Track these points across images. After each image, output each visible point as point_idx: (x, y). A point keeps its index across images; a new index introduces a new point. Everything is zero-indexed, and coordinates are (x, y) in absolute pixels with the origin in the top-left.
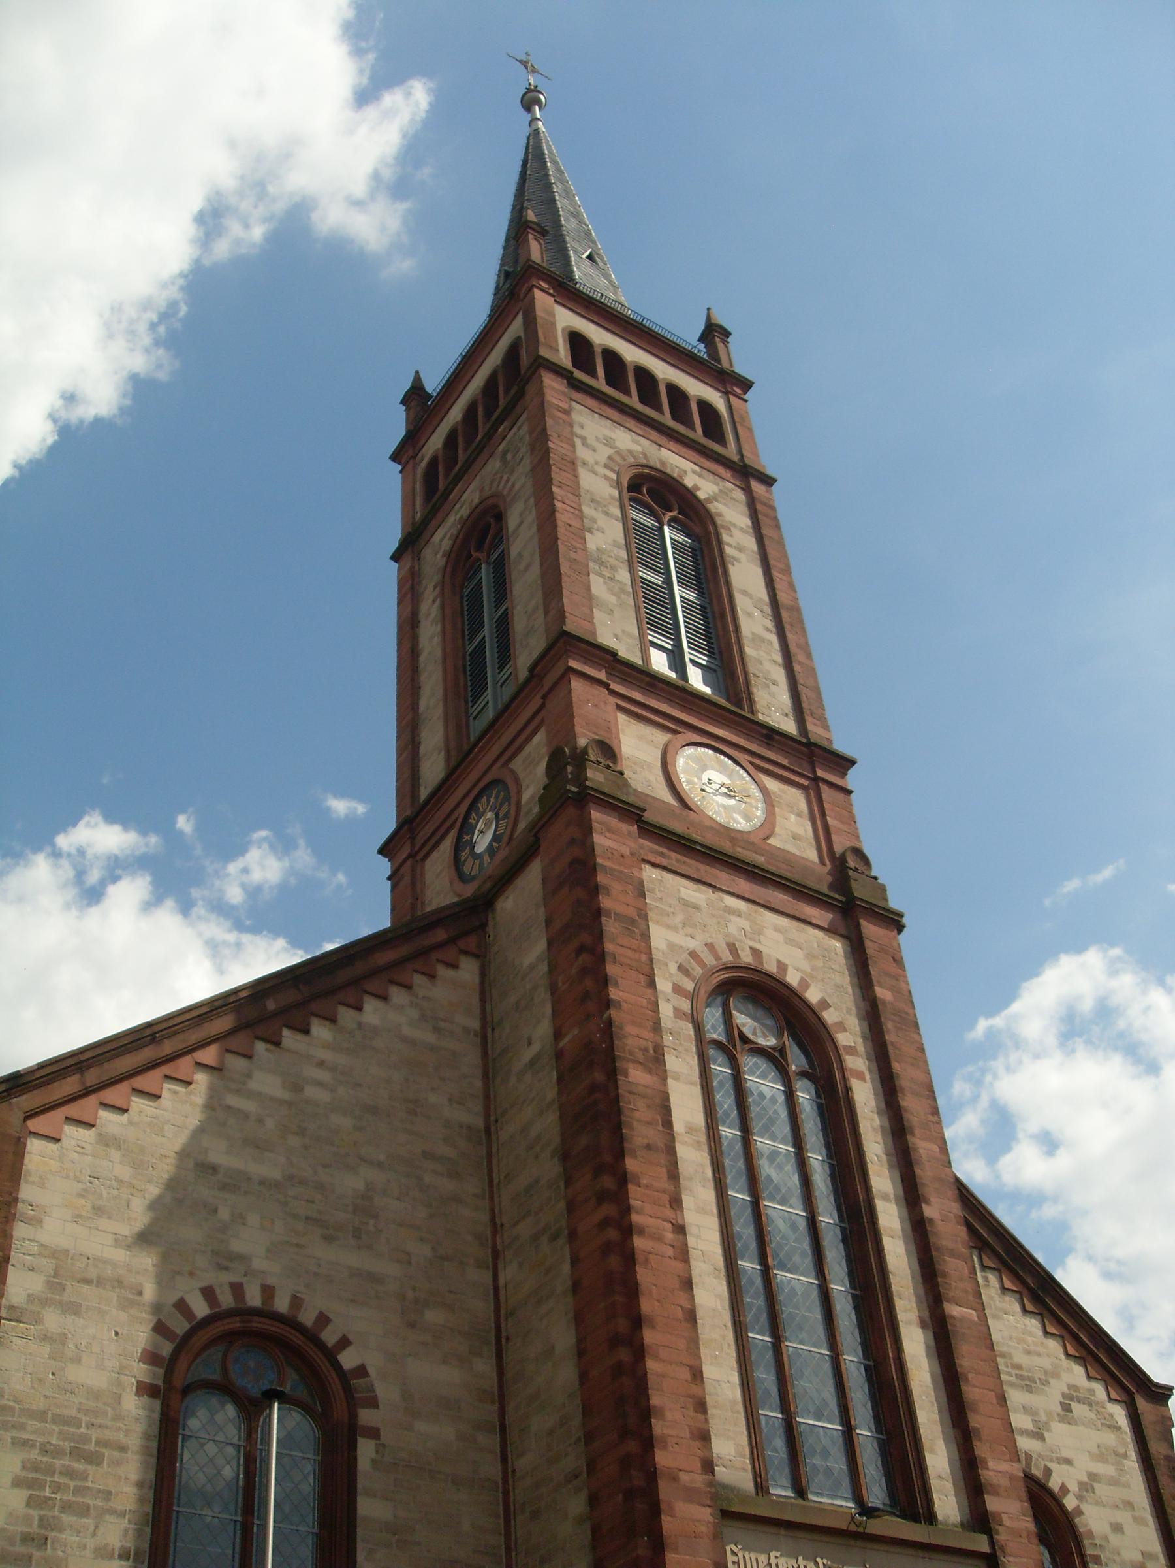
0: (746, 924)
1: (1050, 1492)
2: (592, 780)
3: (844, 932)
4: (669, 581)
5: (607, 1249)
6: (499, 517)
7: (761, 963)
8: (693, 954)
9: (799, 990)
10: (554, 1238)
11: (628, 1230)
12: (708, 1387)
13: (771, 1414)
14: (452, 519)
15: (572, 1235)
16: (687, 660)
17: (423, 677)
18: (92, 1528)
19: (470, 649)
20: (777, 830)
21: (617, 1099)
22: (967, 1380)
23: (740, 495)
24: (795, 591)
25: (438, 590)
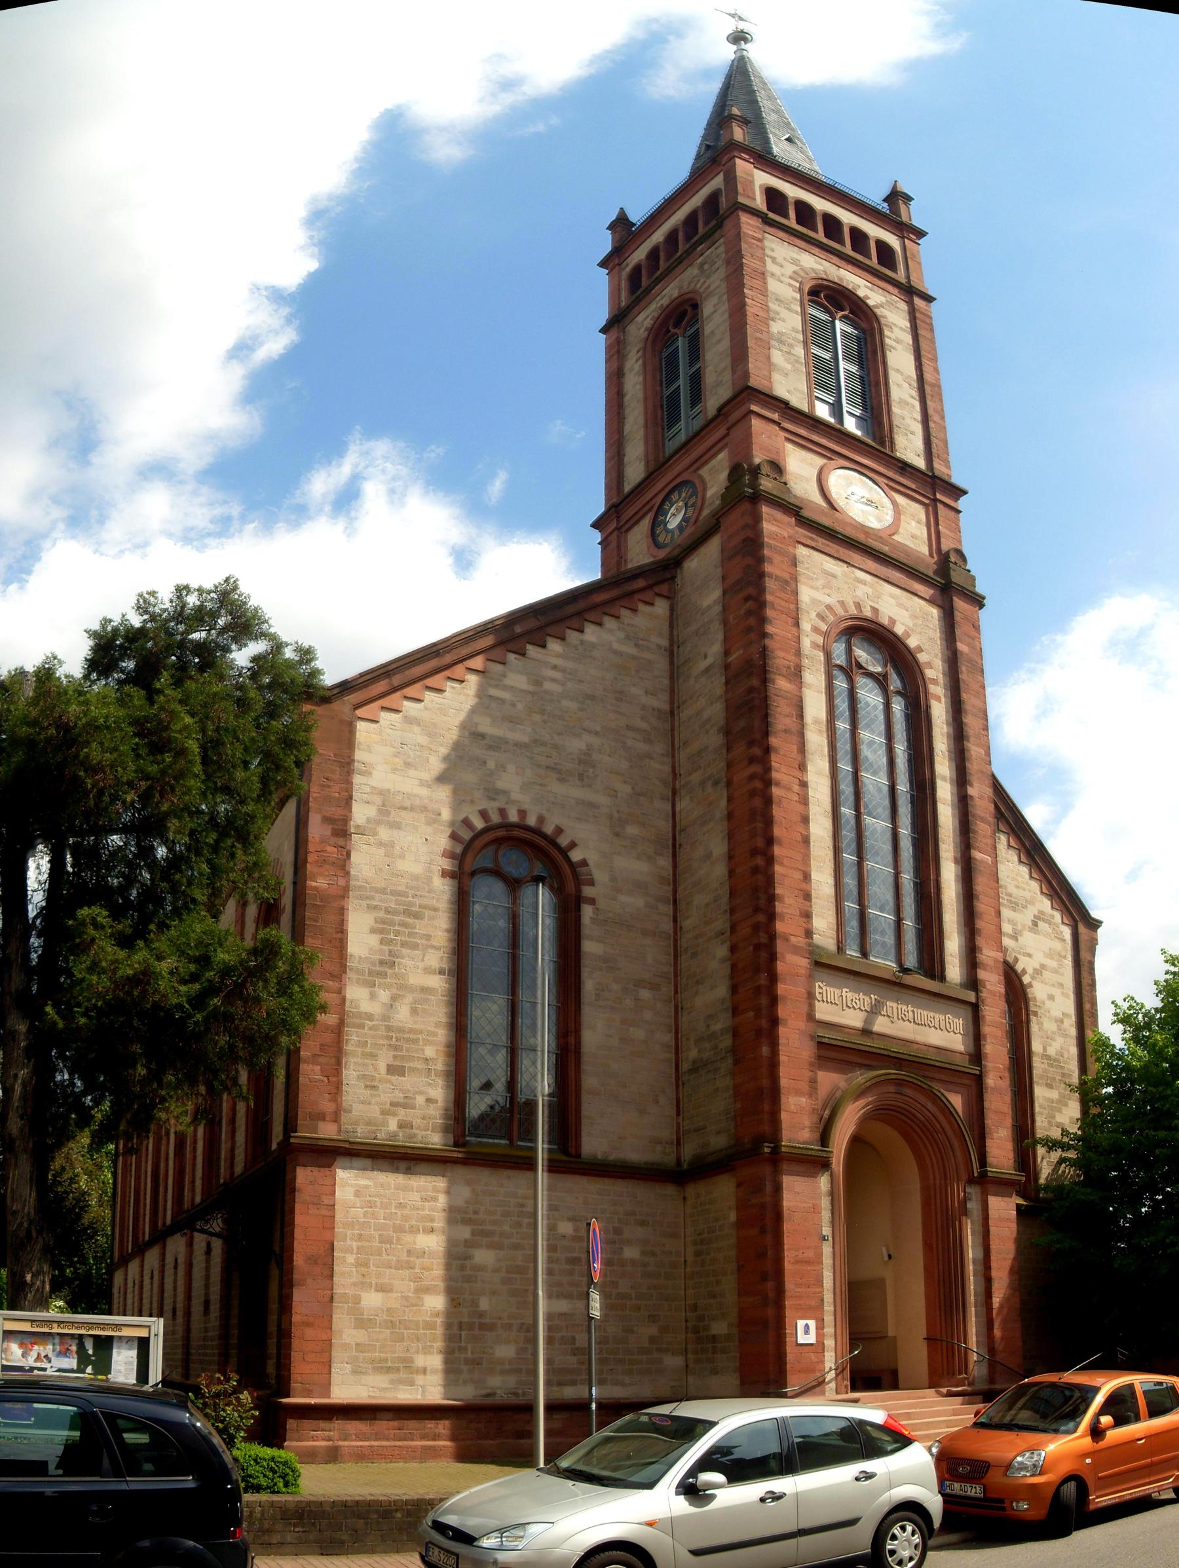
0: (870, 591)
1: (1015, 972)
2: (764, 486)
3: (939, 602)
4: (836, 358)
5: (753, 794)
6: (695, 306)
7: (877, 617)
8: (829, 607)
9: (903, 638)
10: (716, 783)
11: (768, 783)
12: (814, 885)
13: (851, 905)
14: (653, 306)
15: (729, 783)
16: (845, 412)
17: (627, 411)
18: (421, 957)
19: (667, 393)
20: (901, 530)
21: (765, 699)
22: (978, 899)
23: (904, 306)
24: (938, 374)
25: (640, 353)
